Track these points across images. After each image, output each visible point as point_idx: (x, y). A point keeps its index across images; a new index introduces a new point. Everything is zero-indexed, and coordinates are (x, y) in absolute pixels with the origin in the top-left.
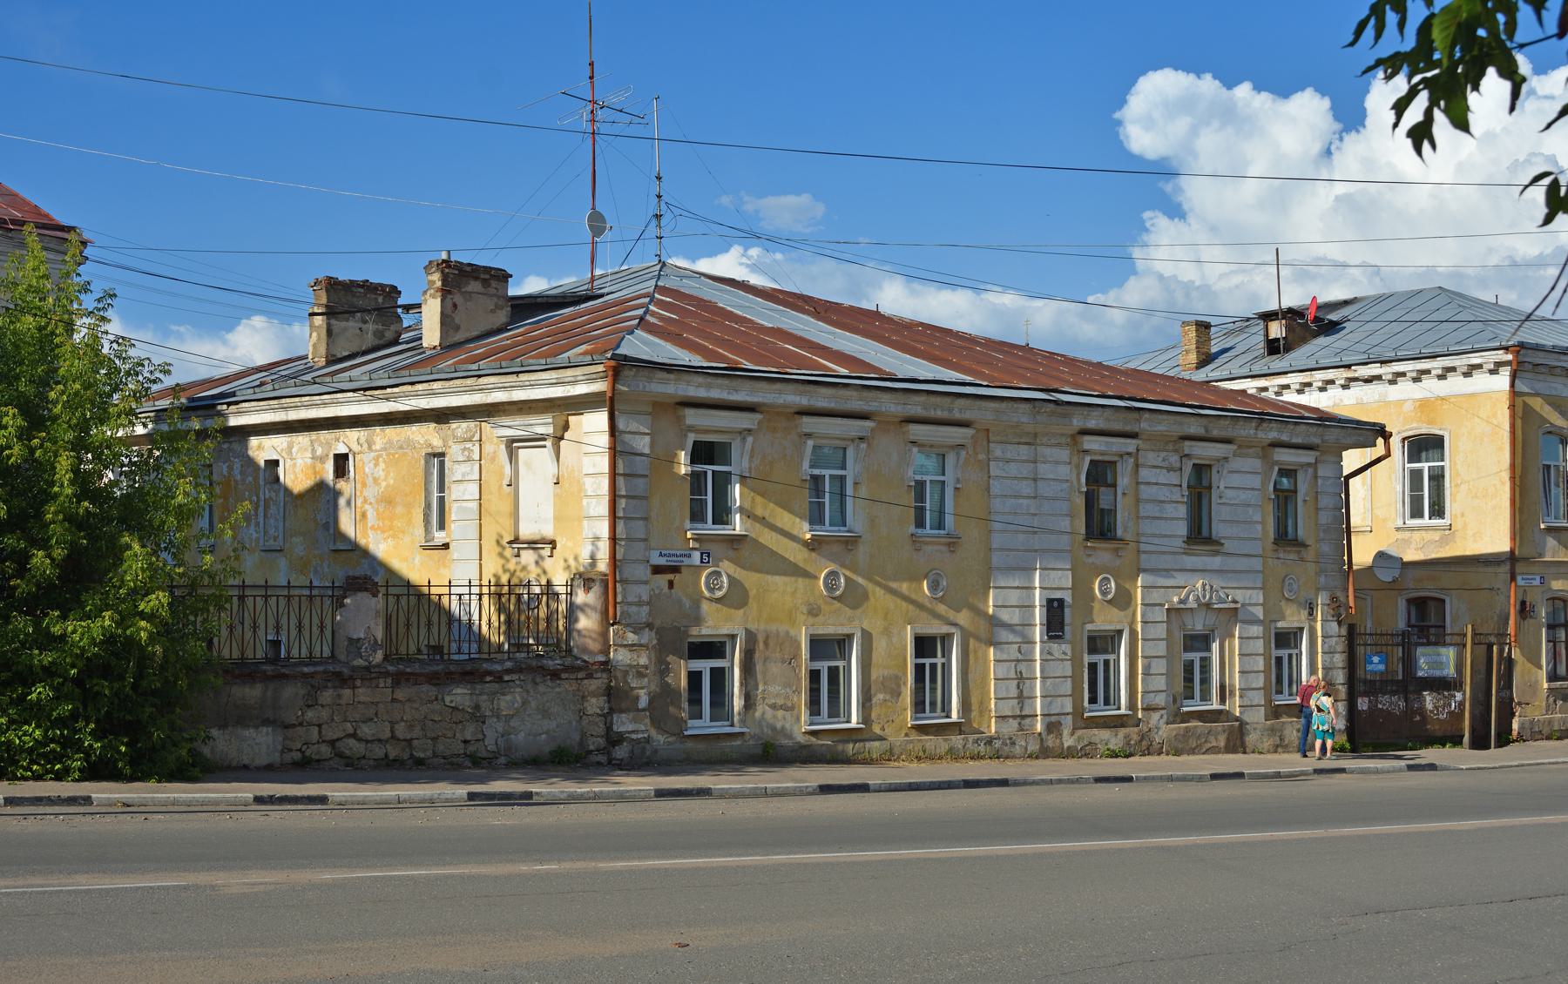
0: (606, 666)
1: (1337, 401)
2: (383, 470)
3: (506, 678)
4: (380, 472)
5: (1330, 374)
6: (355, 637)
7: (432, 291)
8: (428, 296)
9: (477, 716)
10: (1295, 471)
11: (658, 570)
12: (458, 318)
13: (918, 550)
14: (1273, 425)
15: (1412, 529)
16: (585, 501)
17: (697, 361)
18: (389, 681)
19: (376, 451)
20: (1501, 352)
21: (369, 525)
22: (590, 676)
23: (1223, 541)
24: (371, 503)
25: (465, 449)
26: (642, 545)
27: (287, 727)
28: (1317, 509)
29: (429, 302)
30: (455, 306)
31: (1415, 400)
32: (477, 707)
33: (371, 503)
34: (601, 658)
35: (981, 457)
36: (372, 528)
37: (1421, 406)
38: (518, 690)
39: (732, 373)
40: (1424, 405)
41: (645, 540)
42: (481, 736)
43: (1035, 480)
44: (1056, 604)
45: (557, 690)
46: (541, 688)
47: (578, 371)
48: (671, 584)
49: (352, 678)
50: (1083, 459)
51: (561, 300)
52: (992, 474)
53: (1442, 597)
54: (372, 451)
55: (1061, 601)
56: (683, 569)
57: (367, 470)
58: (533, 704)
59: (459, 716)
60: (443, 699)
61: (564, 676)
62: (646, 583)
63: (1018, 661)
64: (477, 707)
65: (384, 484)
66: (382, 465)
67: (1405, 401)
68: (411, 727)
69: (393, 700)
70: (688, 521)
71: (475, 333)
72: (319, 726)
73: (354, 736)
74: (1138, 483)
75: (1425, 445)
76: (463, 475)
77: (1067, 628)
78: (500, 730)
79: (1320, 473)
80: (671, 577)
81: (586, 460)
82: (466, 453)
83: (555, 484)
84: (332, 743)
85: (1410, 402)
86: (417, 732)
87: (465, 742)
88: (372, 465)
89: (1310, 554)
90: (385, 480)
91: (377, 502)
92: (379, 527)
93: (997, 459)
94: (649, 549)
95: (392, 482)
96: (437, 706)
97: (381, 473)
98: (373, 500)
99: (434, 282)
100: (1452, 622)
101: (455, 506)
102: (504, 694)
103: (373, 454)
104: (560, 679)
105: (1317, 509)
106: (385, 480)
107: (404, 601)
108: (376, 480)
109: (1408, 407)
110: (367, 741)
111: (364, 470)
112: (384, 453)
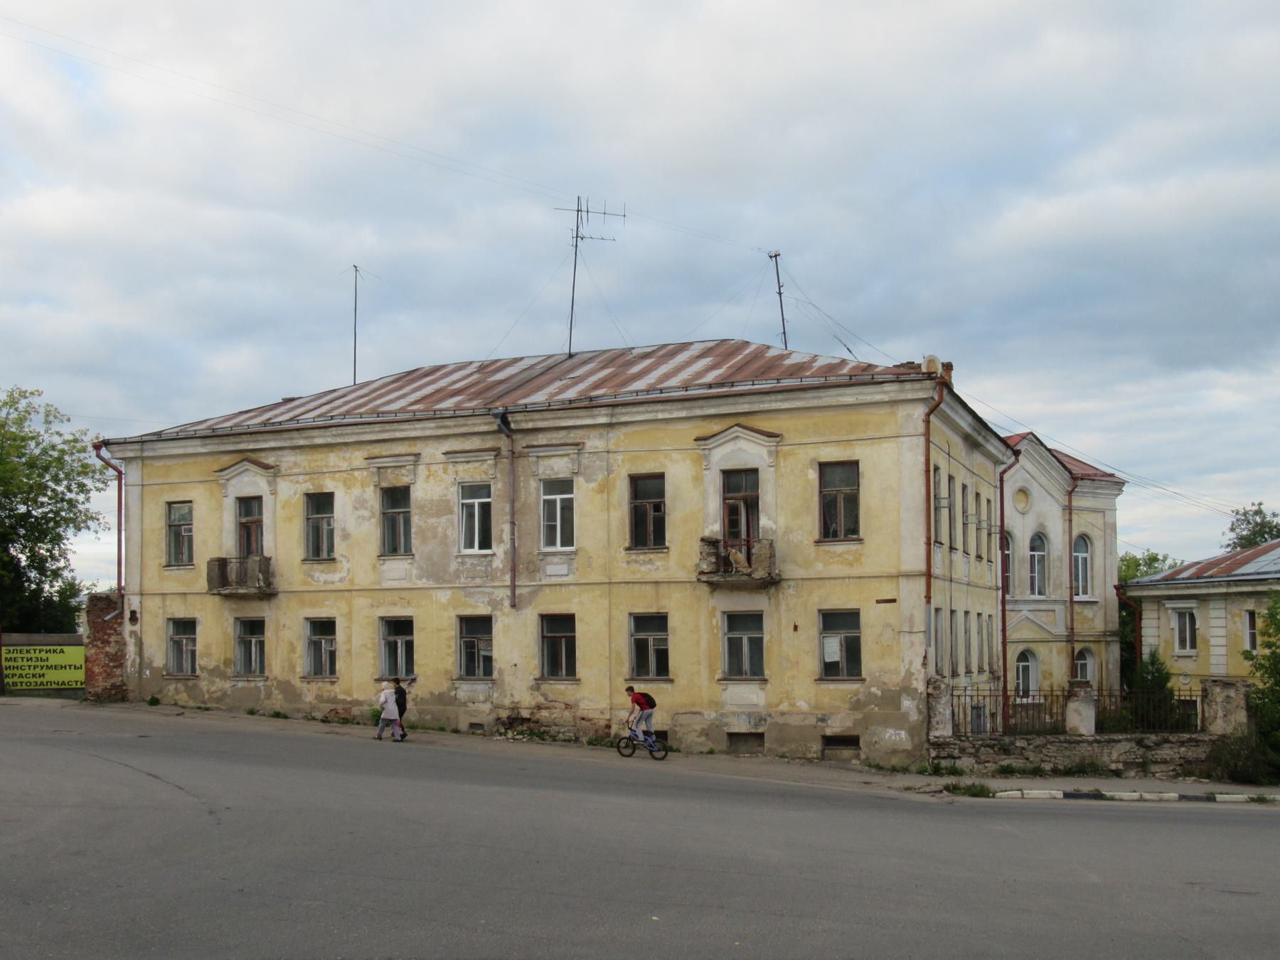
107: (962, 699)
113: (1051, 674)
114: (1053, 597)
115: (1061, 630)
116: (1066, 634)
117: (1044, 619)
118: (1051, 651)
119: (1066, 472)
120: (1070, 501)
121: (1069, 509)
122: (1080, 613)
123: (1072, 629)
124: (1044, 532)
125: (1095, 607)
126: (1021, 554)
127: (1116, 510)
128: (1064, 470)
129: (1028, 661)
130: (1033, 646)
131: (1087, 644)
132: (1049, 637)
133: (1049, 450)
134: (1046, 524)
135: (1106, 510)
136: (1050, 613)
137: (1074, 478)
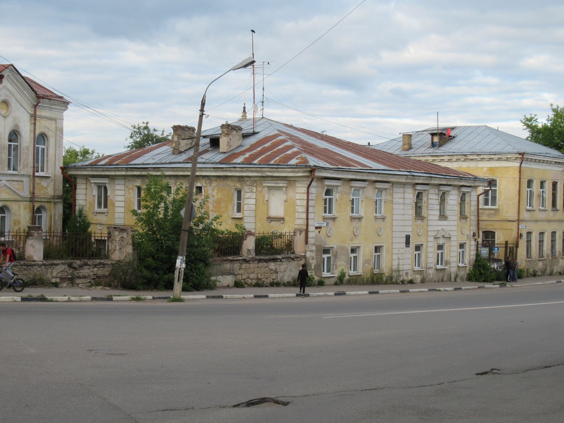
0: (305, 257)
1: (460, 166)
2: (216, 193)
3: (283, 260)
4: (215, 193)
5: (459, 157)
6: (250, 249)
7: (224, 134)
8: (222, 136)
9: (276, 272)
10: (465, 194)
11: (317, 228)
12: (231, 143)
13: (376, 221)
14: (463, 180)
15: (485, 209)
16: (296, 207)
17: (328, 166)
18: (257, 262)
19: (213, 186)
20: (518, 154)
21: (210, 210)
22: (301, 260)
23: (448, 216)
24: (211, 203)
25: (250, 188)
26: (313, 220)
27: (236, 275)
28: (471, 206)
29: (222, 138)
30: (230, 139)
31: (487, 167)
32: (276, 269)
33: (211, 203)
34: (303, 254)
35: (391, 192)
36: (211, 211)
37: (489, 169)
38: (285, 264)
39: (338, 170)
40: (491, 169)
41: (314, 219)
42: (277, 278)
43: (404, 198)
44: (408, 237)
45: (294, 264)
46: (290, 263)
47: (301, 170)
48: (319, 232)
49: (249, 261)
50: (416, 192)
51: (249, 134)
52: (394, 197)
53: (495, 231)
54: (211, 186)
55: (409, 236)
56: (322, 228)
57: (209, 192)
58: (289, 268)
59: (272, 271)
60: (269, 267)
61: (295, 259)
62: (314, 232)
63: (398, 254)
64: (276, 269)
65: (216, 197)
66: (216, 191)
67: (484, 167)
68: (261, 275)
69: (258, 267)
70: (323, 213)
71: (235, 148)
72: (242, 275)
73: (248, 278)
74: (428, 199)
75: (492, 183)
76: (249, 196)
77: (410, 244)
78: (281, 276)
79: (472, 194)
80: (319, 230)
81: (297, 195)
82: (251, 190)
83: (285, 201)
84: (244, 280)
85: (485, 168)
86: (263, 277)
87: (273, 279)
88: (211, 191)
89: (468, 220)
90: (217, 196)
91: (213, 202)
92: (214, 211)
93: (395, 192)
94: (314, 222)
95: (220, 197)
96: (267, 269)
97: (215, 193)
98: (212, 202)
99: (224, 131)
100: (497, 239)
101: (246, 206)
102: (282, 265)
103: (212, 187)
104: (294, 260)
105: (471, 206)
106: (217, 196)
108: (213, 196)
109: (485, 169)
110: (252, 279)
111: (208, 192)
112: (217, 187)
113: (19, 222)
114: (22, 173)
115: (26, 194)
116: (30, 196)
117: (16, 186)
118: (20, 207)
119: (33, 93)
120: (35, 111)
121: (34, 117)
122: (39, 184)
123: (34, 193)
124: (18, 130)
125: (48, 180)
126: (2, 144)
127: (63, 119)
128: (32, 91)
129: (5, 214)
130: (8, 204)
131: (43, 204)
132: (19, 198)
133: (23, 78)
134: (19, 125)
135: (57, 119)
136: (20, 183)
137: (39, 97)
